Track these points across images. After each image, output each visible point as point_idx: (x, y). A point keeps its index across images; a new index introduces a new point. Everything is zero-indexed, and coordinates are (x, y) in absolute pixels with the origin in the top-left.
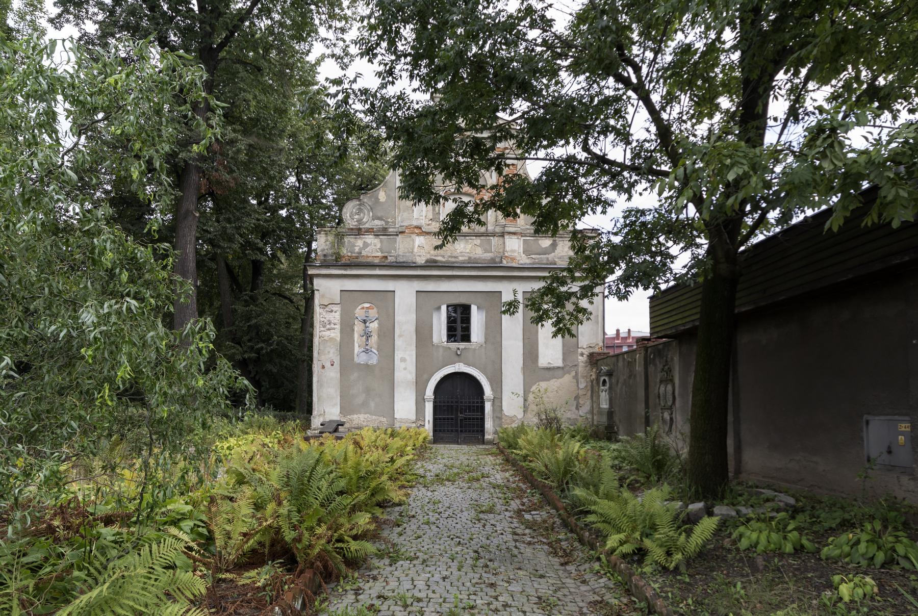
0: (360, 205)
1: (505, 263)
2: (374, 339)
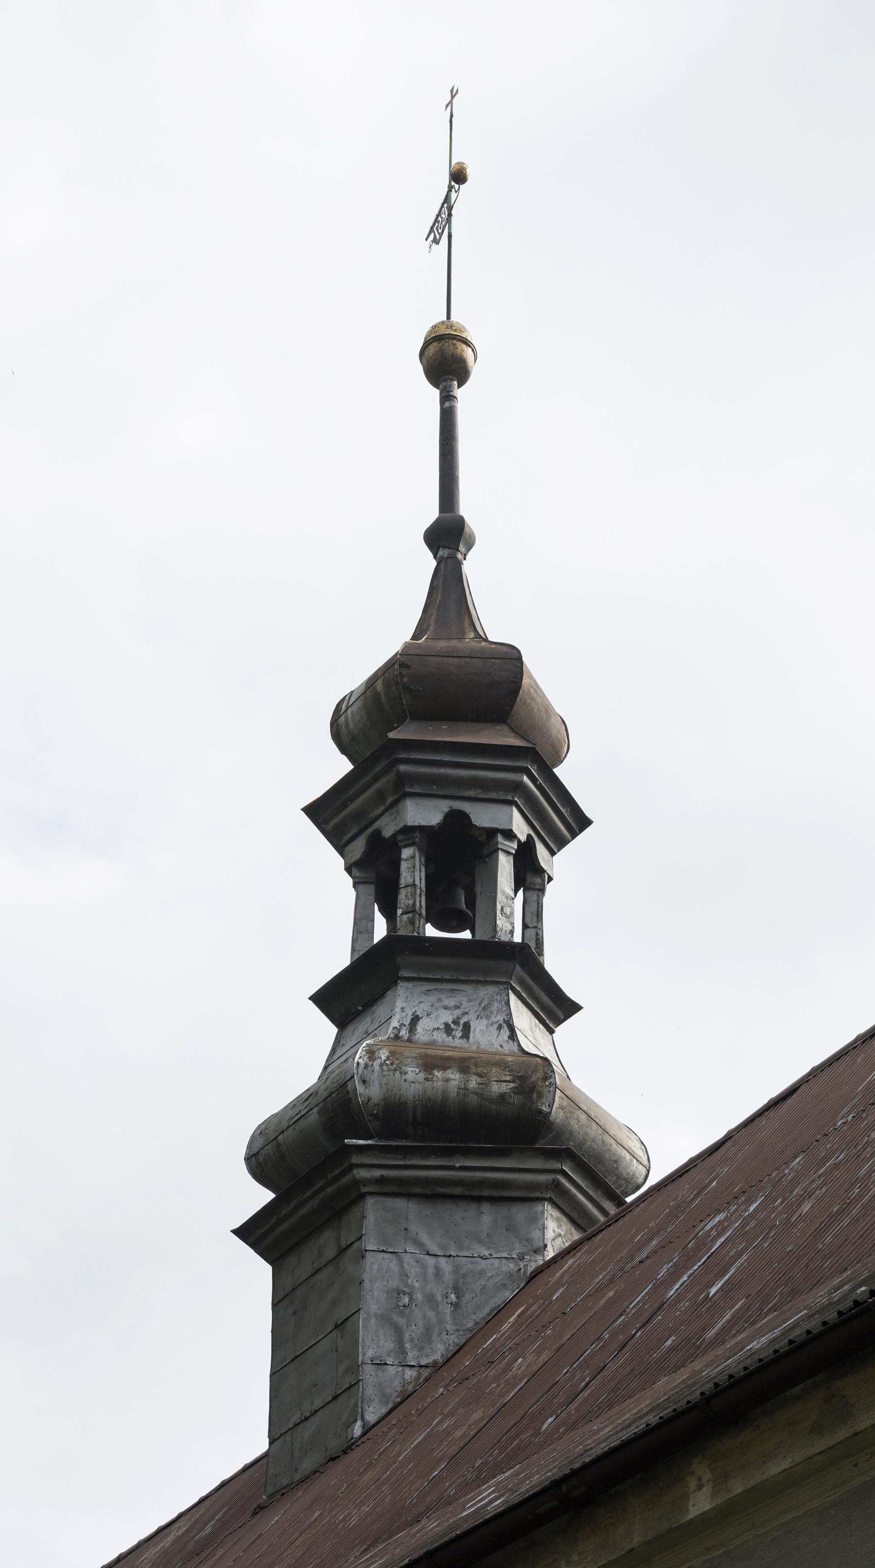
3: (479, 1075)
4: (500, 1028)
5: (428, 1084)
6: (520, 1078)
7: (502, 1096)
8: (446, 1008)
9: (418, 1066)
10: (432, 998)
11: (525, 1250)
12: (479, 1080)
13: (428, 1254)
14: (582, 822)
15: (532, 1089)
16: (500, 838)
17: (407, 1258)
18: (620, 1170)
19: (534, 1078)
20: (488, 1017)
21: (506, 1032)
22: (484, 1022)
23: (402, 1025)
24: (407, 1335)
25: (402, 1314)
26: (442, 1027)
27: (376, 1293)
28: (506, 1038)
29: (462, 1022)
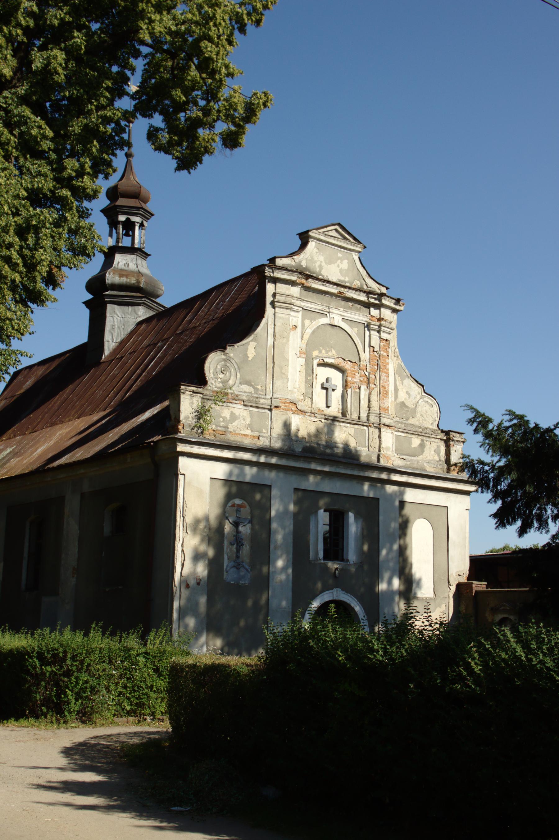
0: (225, 360)
1: (320, 277)
2: (246, 549)
14: (153, 215)
17: (115, 318)
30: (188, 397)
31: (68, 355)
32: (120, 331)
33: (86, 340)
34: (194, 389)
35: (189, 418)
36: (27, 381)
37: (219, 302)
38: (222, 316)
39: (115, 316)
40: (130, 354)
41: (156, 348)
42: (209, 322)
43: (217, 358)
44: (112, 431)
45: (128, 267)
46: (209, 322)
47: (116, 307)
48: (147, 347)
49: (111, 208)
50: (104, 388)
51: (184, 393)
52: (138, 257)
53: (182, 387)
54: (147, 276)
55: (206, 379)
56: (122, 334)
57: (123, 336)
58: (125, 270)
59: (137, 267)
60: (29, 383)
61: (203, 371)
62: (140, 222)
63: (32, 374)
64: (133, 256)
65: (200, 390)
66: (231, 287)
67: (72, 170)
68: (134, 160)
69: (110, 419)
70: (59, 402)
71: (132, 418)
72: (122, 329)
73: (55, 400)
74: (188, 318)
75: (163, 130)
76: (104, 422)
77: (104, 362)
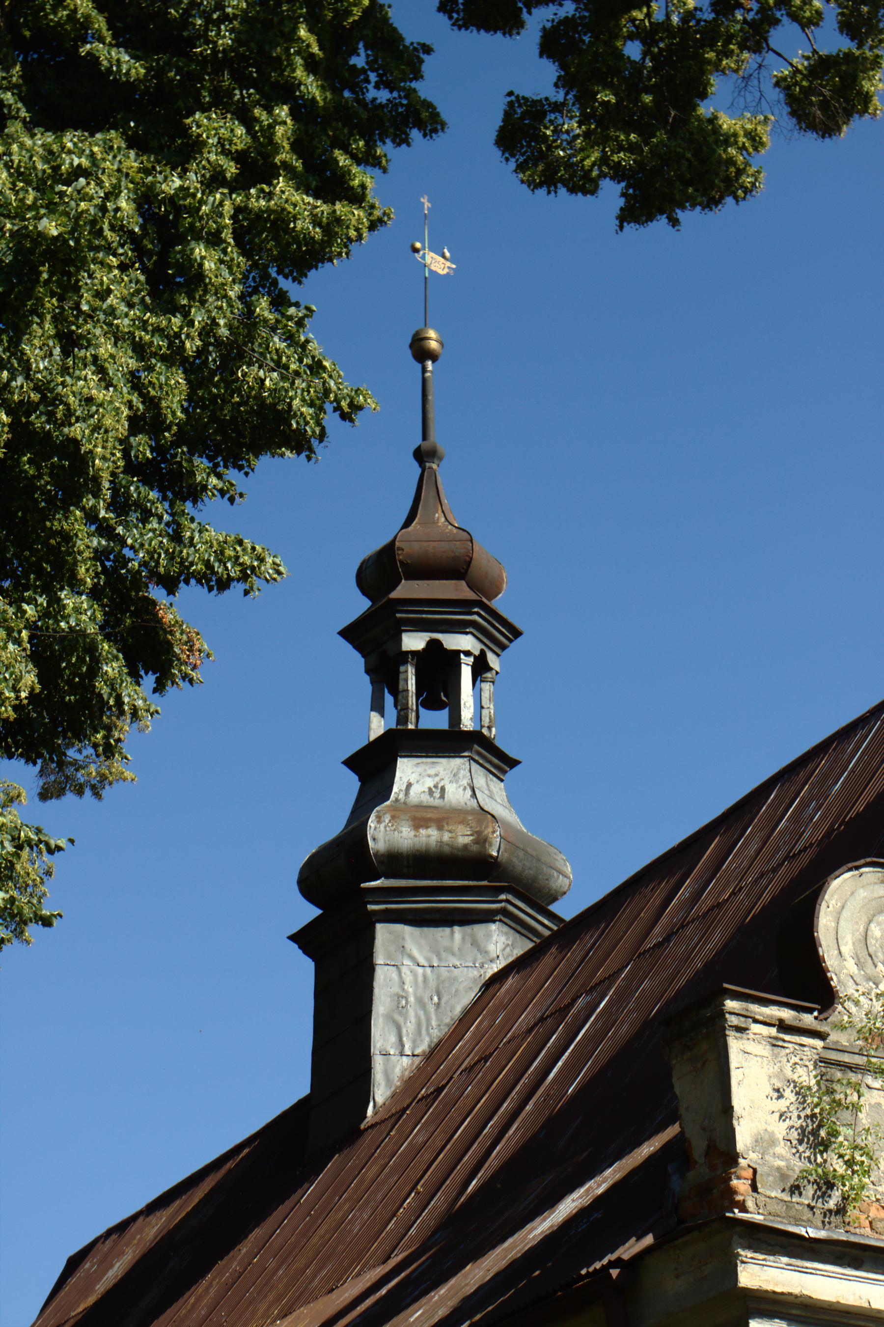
3: (450, 831)
4: (465, 789)
5: (416, 839)
6: (477, 832)
7: (466, 846)
8: (429, 776)
9: (409, 827)
10: (420, 769)
11: (484, 960)
12: (450, 835)
13: (418, 965)
14: (516, 633)
15: (485, 840)
16: (462, 656)
17: (404, 970)
18: (720, 122)
19: (486, 832)
20: (457, 782)
21: (469, 792)
22: (455, 785)
23: (401, 790)
24: (404, 1031)
25: (400, 1014)
26: (427, 790)
27: (383, 998)
28: (469, 797)
29: (440, 786)
30: (764, 1050)
31: (246, 1151)
32: (426, 1013)
33: (304, 1090)
34: (786, 1014)
35: (773, 1142)
36: (111, 1266)
37: (804, 805)
38: (828, 834)
39: (407, 962)
40: (470, 1069)
41: (568, 1019)
42: (775, 870)
43: (862, 894)
44: (424, 1300)
45: (442, 796)
46: (775, 870)
47: (407, 930)
48: (530, 1031)
49: (373, 611)
50: (379, 1197)
51: (741, 1030)
52: (475, 766)
53: (731, 1004)
54: (506, 825)
55: (828, 980)
56: (434, 1023)
57: (436, 1032)
58: (434, 807)
59: (474, 794)
60: (117, 1270)
61: (811, 945)
62: (477, 653)
63: (127, 1245)
64: (458, 761)
65: (808, 1020)
66: (844, 751)
67: (225, 153)
68: (441, 470)
69: (408, 1276)
70: (212, 1292)
71: (503, 1240)
72: (432, 1009)
73: (200, 1290)
74: (684, 892)
75: (557, 107)
76: (384, 1291)
77: (372, 1127)
